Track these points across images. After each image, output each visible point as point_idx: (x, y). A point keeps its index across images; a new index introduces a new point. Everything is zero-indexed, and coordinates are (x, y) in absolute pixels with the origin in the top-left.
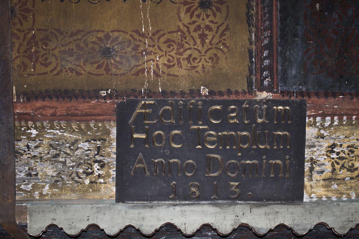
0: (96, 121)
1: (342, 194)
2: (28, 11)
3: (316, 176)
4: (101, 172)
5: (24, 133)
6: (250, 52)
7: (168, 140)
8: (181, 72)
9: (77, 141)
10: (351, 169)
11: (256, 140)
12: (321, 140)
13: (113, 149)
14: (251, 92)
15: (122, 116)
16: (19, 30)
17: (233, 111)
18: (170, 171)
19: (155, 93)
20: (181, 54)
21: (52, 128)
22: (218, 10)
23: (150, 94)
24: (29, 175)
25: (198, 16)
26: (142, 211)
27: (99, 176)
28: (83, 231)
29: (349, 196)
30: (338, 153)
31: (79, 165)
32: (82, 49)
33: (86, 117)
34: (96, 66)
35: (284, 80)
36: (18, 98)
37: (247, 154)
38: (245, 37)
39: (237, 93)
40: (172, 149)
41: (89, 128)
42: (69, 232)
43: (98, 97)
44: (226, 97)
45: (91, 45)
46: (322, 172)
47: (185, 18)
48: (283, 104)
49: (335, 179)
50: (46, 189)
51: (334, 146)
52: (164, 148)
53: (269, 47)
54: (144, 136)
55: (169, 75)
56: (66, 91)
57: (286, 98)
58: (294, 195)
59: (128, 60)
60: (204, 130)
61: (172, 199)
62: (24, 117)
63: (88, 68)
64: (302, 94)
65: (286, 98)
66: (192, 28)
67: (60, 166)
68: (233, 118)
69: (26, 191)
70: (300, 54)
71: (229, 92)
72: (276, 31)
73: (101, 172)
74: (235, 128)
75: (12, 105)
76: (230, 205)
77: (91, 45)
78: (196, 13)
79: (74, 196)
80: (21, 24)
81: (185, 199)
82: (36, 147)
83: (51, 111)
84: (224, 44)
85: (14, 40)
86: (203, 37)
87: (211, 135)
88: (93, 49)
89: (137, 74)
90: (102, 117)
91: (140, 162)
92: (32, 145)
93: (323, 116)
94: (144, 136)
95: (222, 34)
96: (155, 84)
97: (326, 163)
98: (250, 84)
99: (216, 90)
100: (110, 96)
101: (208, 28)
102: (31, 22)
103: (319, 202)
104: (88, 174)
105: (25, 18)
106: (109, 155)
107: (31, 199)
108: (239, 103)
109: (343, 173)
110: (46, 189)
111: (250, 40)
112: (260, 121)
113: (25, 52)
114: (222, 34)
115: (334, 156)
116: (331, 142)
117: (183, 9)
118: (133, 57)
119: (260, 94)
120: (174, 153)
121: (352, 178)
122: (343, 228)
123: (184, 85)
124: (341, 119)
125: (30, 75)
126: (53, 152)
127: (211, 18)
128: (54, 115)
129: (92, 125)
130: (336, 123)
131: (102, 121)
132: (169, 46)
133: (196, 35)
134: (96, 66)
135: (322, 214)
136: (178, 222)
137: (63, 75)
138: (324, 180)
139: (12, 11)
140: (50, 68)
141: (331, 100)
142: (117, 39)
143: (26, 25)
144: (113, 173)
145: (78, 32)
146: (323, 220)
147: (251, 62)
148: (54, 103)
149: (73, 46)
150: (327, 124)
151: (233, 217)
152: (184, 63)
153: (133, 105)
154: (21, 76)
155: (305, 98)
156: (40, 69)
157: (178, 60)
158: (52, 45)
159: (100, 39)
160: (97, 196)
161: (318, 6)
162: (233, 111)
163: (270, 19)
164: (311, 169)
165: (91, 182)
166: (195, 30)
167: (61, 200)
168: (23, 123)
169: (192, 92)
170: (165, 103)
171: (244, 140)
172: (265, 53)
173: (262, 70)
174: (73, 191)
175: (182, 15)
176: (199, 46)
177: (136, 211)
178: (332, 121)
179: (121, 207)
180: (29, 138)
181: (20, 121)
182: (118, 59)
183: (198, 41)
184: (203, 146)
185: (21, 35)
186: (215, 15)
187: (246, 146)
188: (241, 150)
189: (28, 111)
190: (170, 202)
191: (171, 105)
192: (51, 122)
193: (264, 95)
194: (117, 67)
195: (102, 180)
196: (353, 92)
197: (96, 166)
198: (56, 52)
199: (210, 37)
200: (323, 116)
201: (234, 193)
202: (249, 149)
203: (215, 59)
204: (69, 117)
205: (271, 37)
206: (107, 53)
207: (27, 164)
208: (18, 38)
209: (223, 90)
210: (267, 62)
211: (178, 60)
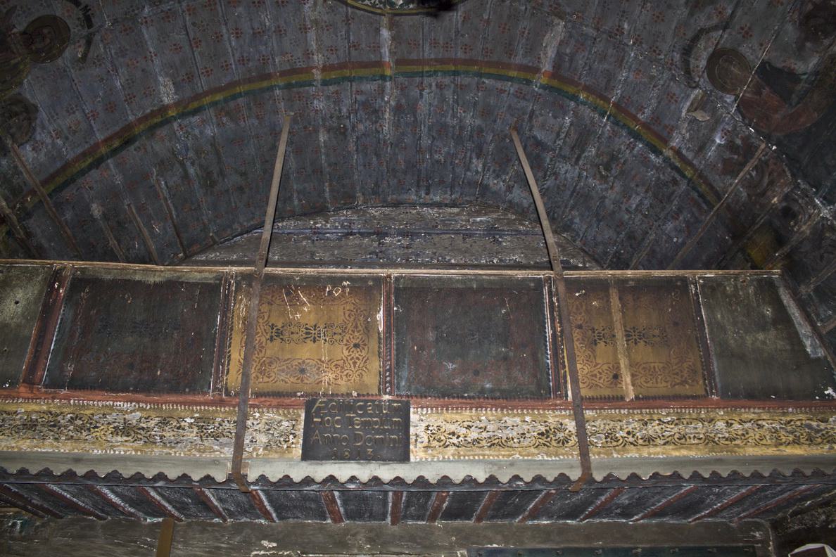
0: (294, 409)
1: (435, 456)
2: (263, 347)
3: (418, 444)
4: (293, 441)
5: (252, 415)
6: (380, 372)
7: (333, 422)
8: (342, 382)
9: (281, 420)
10: (439, 441)
11: (382, 424)
12: (421, 420)
13: (301, 426)
14: (380, 395)
15: (309, 407)
16: (257, 358)
17: (370, 406)
18: (333, 441)
19: (327, 395)
20: (343, 372)
21: (268, 412)
22: (363, 349)
23: (325, 395)
24: (252, 441)
25: (353, 352)
26: (316, 467)
27: (293, 443)
28: (280, 479)
29: (438, 458)
30: (431, 431)
31: (281, 436)
32: (289, 369)
33: (287, 407)
34: (296, 378)
35: (398, 388)
36: (252, 396)
37: (378, 432)
38: (377, 364)
39: (372, 395)
40: (334, 428)
41: (289, 413)
42: (272, 480)
43: (296, 396)
44: (366, 398)
45: (294, 367)
46: (422, 442)
47: (346, 353)
48: (397, 402)
49: (430, 447)
50: (261, 452)
51: (429, 426)
52: (330, 427)
53: (390, 370)
54: (319, 420)
55: (336, 384)
56: (279, 393)
57: (399, 399)
58: (404, 457)
59: (314, 375)
60: (354, 417)
61: (335, 459)
62: (253, 406)
63: (292, 379)
64: (408, 396)
65: (399, 399)
66: (349, 358)
67: (270, 436)
68: (369, 410)
69: (248, 452)
70: (407, 373)
71: (368, 395)
72: (394, 361)
73: (293, 441)
74: (371, 416)
75: (248, 399)
76: (367, 463)
77: (294, 367)
78: (352, 350)
79: (276, 456)
80: (258, 354)
81: (341, 460)
82: (258, 424)
83: (269, 403)
84: (366, 368)
85: (254, 363)
86: (355, 363)
87: (357, 420)
88: (295, 369)
89: (318, 383)
90: (296, 407)
91: (317, 435)
92: (255, 422)
93: (422, 408)
94: (319, 420)
95: (365, 362)
96: (328, 389)
97: (425, 436)
98: (379, 390)
99: (361, 393)
100: (302, 396)
101: (358, 358)
102: (263, 353)
103: (420, 463)
104: (286, 442)
105: (261, 351)
106: (299, 430)
107: (251, 458)
108: (373, 401)
109: (435, 443)
110: (261, 452)
111: (380, 365)
112: (384, 412)
113: (259, 370)
114: (365, 362)
115: (429, 432)
116: (427, 424)
117: (345, 348)
118: (317, 373)
119: (364, 286)
120: (336, 430)
121: (440, 446)
122: (434, 479)
123: (343, 390)
124: (432, 409)
125: (260, 383)
126: (267, 427)
127: (360, 353)
128: (270, 405)
129: (291, 411)
130: (429, 412)
131: (297, 409)
132: (336, 368)
133: (351, 362)
134: (296, 378)
135: (421, 470)
136: (336, 475)
137: (278, 383)
138: (424, 447)
139: (255, 347)
140: (271, 379)
141: (424, 399)
142: (309, 363)
143: (261, 355)
144: (301, 442)
145: (288, 359)
146: (422, 474)
147: (381, 378)
148: (271, 399)
149: (285, 367)
150: (424, 413)
151: (369, 471)
152: (344, 378)
153: (314, 401)
154: (255, 383)
155: (410, 399)
156: (266, 379)
157: (341, 376)
158: (273, 366)
159: (299, 363)
160: (290, 456)
161: (416, 348)
162: (370, 406)
163: (390, 355)
164: (416, 440)
165: (288, 447)
166: (351, 359)
167: (269, 458)
168: (252, 409)
169: (348, 394)
170: (332, 400)
171: (376, 423)
172: (388, 374)
173: (386, 383)
174: (276, 452)
175: (344, 351)
176: (352, 368)
177: (313, 467)
178: (427, 411)
179: (304, 464)
180: (254, 419)
181: (250, 408)
182: (308, 375)
183: (352, 366)
184: (353, 427)
185: (257, 360)
186: (361, 351)
187: (377, 427)
188: (374, 429)
189: (257, 403)
190: (333, 461)
191: (335, 402)
192: (268, 408)
193: (387, 397)
194: (307, 380)
195: (294, 446)
196: (436, 395)
197: (291, 437)
198: (275, 370)
199: (358, 363)
200: (422, 408)
201: (370, 456)
202: (378, 429)
203: (361, 375)
204: (278, 406)
205: (391, 365)
206: (303, 371)
207: (251, 434)
208: (256, 362)
209: (365, 393)
210: (388, 379)
211: (341, 376)
